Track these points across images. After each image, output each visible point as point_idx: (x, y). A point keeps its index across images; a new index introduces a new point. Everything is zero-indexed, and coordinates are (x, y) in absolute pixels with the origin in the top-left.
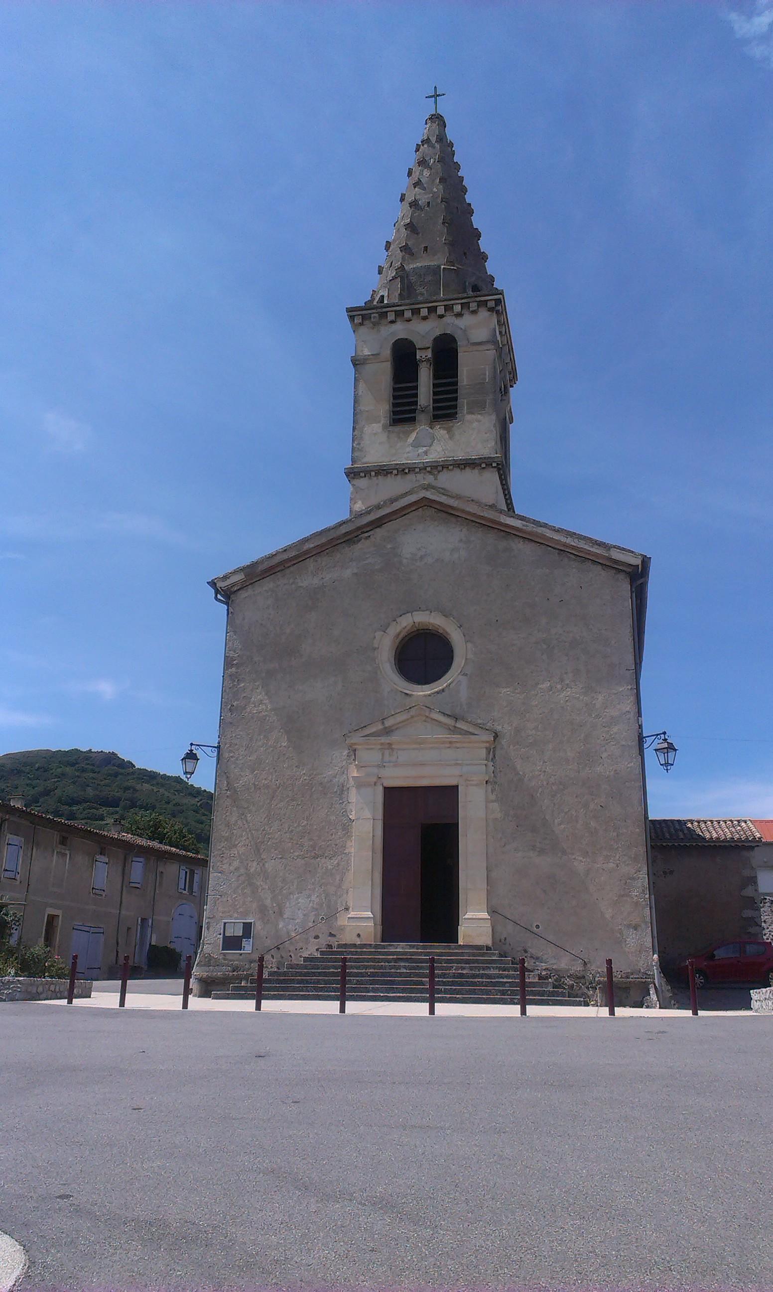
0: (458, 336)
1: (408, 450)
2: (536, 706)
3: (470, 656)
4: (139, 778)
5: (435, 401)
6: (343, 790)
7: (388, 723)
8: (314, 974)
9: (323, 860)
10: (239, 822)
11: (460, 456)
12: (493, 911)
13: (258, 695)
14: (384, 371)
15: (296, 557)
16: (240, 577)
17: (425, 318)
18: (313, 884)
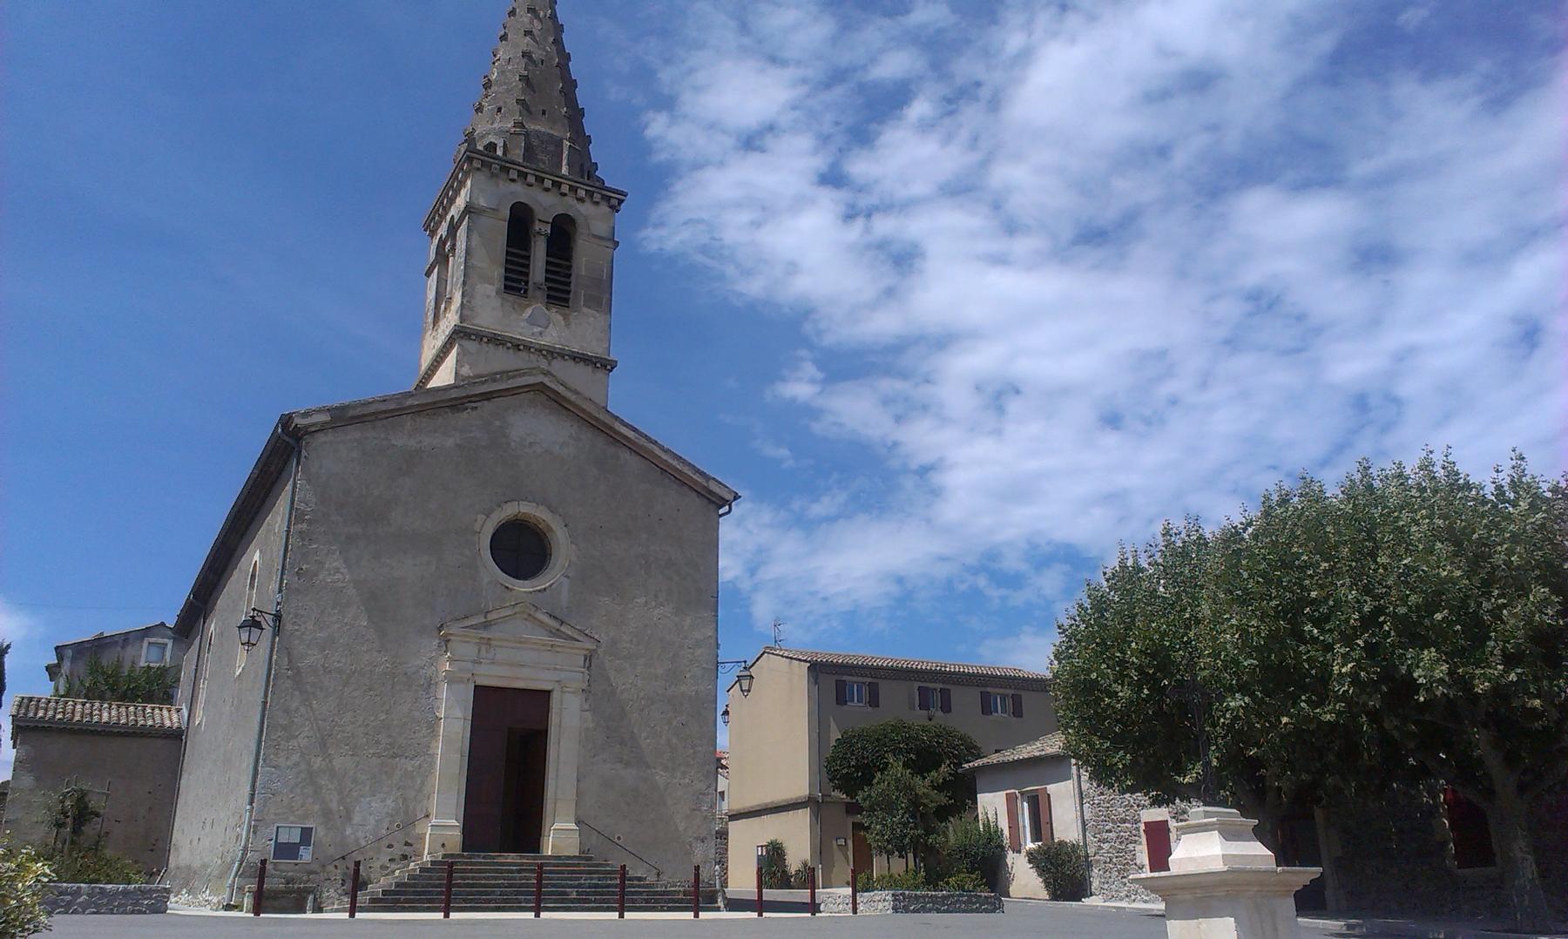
0: (580, 221)
3: (574, 559)
6: (430, 685)
7: (490, 617)
10: (302, 709)
13: (335, 562)
14: (499, 229)
16: (325, 418)
17: (547, 190)
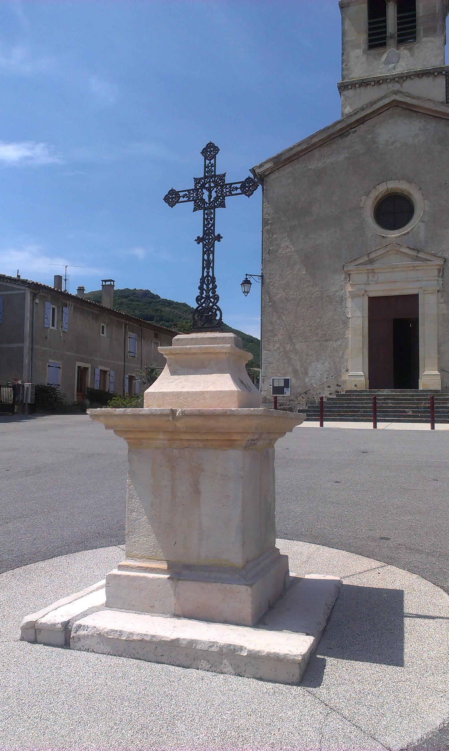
1: (381, 67)
3: (427, 209)
4: (162, 304)
5: (399, 30)
6: (342, 300)
8: (336, 407)
9: (331, 342)
11: (419, 68)
12: (441, 370)
13: (286, 242)
15: (306, 149)
16: (270, 165)
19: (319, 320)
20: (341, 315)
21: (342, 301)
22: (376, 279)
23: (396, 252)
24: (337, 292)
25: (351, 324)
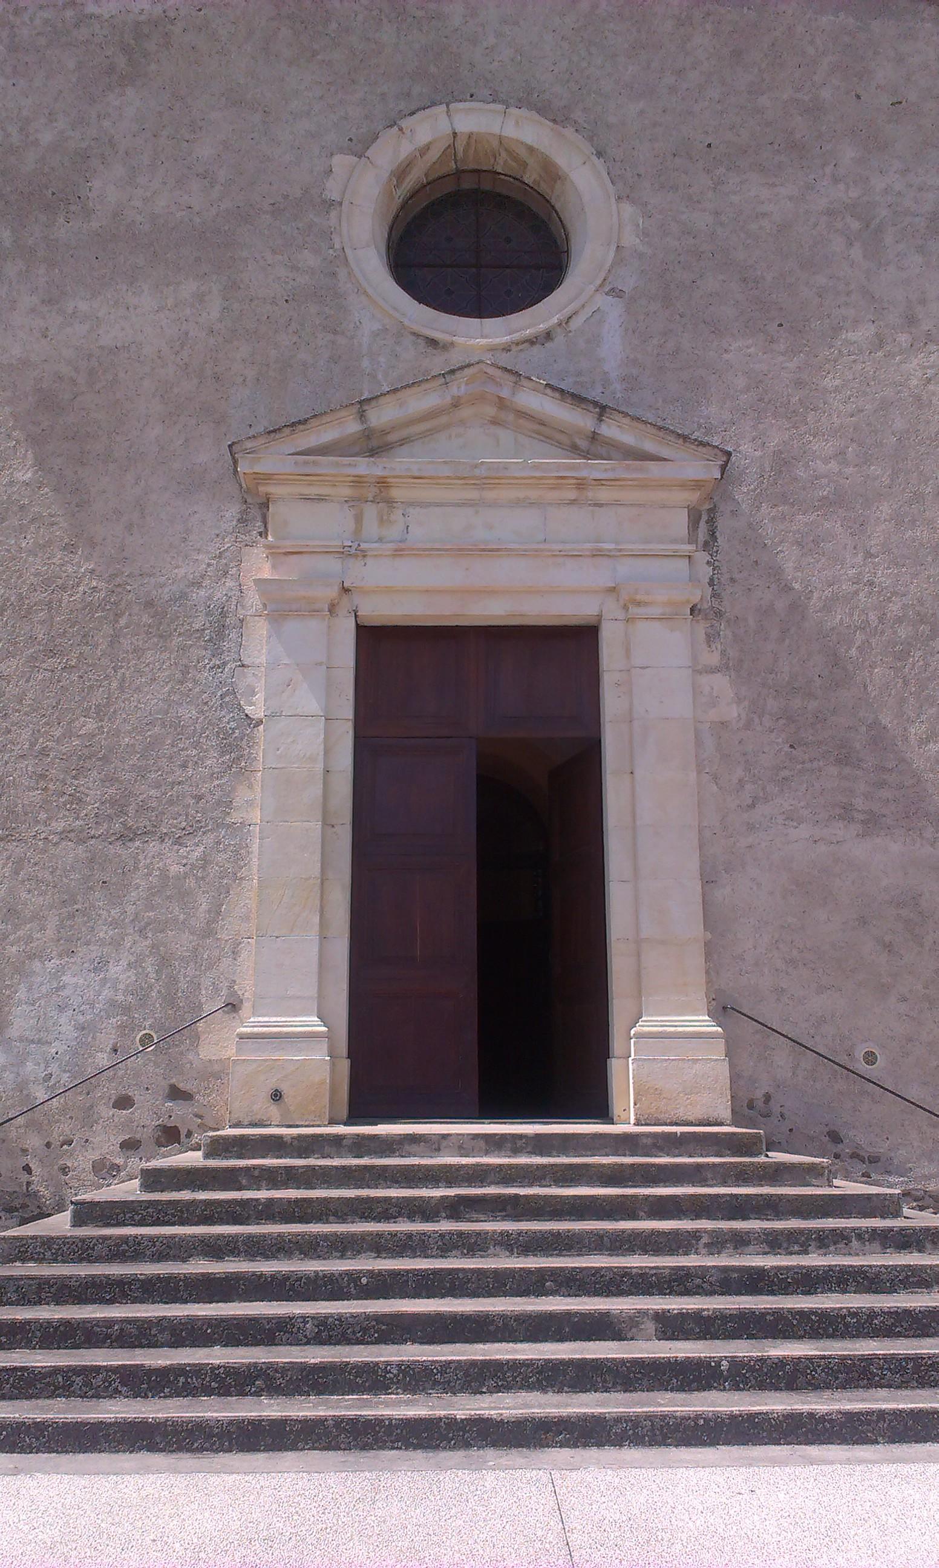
2: (837, 390)
3: (630, 239)
6: (222, 627)
7: (382, 416)
9: (153, 847)
12: (723, 1009)
18: (114, 924)
19: (91, 725)
20: (215, 701)
21: (221, 630)
22: (394, 532)
23: (491, 411)
24: (199, 585)
25: (263, 749)
